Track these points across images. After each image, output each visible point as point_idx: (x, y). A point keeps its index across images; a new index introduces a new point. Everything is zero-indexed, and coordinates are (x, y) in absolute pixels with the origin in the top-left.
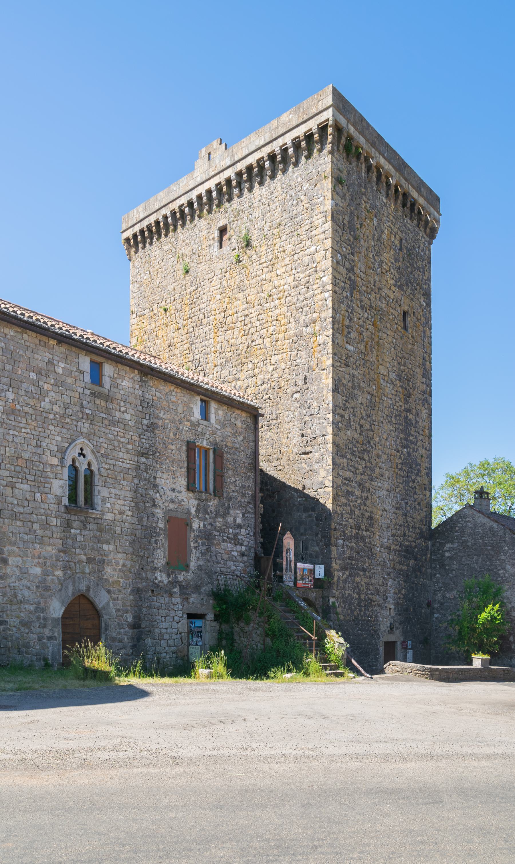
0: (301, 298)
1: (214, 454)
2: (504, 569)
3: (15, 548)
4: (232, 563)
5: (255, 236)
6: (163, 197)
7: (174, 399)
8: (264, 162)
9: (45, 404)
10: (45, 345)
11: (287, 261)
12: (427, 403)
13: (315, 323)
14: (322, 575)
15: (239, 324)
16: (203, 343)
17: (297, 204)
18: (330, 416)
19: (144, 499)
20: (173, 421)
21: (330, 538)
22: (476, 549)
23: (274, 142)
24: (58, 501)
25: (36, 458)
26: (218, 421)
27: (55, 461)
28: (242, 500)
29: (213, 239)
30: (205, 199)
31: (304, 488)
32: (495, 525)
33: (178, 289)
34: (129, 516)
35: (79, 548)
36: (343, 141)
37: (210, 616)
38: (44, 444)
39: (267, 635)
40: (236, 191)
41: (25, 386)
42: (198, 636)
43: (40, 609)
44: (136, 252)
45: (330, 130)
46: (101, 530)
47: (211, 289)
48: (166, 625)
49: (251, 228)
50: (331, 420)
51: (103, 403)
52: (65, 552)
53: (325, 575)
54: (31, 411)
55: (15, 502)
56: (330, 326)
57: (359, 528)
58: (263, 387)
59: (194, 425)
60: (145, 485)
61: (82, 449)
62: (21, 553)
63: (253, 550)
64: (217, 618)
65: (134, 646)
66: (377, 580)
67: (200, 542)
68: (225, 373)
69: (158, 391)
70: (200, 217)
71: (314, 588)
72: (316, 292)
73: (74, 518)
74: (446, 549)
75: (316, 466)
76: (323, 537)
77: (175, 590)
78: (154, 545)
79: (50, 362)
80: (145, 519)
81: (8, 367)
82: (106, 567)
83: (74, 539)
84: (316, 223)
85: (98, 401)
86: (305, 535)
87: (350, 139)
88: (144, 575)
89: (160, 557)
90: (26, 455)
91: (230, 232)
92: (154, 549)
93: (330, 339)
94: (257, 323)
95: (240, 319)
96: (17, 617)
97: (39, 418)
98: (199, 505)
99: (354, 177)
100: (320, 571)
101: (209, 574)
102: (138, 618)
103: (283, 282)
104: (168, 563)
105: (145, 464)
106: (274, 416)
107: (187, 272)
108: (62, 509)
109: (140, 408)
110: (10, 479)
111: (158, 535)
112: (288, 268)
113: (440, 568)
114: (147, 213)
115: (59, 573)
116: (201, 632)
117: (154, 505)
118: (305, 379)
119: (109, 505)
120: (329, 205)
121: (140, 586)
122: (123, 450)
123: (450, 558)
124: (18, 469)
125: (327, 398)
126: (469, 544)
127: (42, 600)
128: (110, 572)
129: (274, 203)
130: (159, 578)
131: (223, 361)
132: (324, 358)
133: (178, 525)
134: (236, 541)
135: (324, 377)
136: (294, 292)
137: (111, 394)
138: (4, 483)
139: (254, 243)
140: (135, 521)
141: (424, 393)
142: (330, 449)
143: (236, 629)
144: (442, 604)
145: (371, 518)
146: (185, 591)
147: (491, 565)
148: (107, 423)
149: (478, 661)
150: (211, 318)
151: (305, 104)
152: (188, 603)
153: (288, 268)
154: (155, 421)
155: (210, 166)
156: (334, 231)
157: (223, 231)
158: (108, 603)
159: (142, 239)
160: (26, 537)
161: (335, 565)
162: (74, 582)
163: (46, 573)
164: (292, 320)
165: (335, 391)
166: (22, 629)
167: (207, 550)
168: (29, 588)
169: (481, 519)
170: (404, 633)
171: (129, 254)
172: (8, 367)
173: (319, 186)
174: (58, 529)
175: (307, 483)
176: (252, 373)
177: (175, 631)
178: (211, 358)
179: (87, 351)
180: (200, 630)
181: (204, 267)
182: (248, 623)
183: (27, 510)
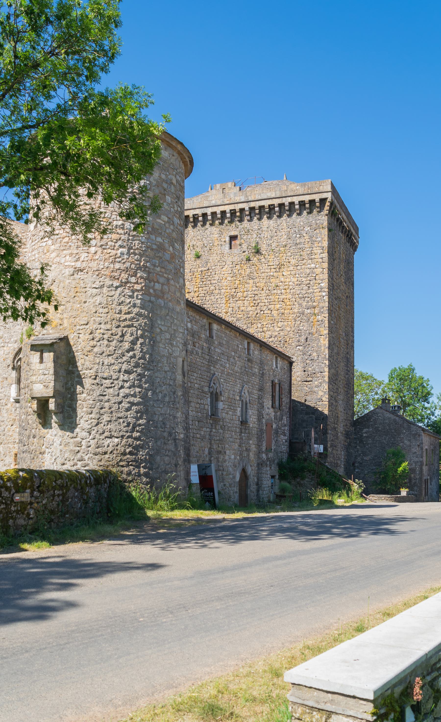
0: (304, 292)
2: (403, 442)
5: (263, 248)
11: (292, 268)
13: (315, 308)
18: (327, 362)
22: (384, 432)
31: (306, 401)
37: (277, 477)
45: (328, 204)
49: (260, 242)
50: (327, 364)
66: (339, 452)
72: (315, 291)
74: (363, 431)
75: (316, 389)
103: (288, 280)
112: (292, 273)
113: (360, 443)
118: (307, 338)
120: (325, 244)
123: (366, 437)
125: (324, 352)
126: (380, 429)
132: (321, 329)
135: (321, 339)
136: (297, 288)
144: (361, 464)
147: (394, 441)
149: (404, 492)
151: (310, 184)
157: (233, 238)
161: (329, 445)
175: (308, 398)
182: (303, 479)
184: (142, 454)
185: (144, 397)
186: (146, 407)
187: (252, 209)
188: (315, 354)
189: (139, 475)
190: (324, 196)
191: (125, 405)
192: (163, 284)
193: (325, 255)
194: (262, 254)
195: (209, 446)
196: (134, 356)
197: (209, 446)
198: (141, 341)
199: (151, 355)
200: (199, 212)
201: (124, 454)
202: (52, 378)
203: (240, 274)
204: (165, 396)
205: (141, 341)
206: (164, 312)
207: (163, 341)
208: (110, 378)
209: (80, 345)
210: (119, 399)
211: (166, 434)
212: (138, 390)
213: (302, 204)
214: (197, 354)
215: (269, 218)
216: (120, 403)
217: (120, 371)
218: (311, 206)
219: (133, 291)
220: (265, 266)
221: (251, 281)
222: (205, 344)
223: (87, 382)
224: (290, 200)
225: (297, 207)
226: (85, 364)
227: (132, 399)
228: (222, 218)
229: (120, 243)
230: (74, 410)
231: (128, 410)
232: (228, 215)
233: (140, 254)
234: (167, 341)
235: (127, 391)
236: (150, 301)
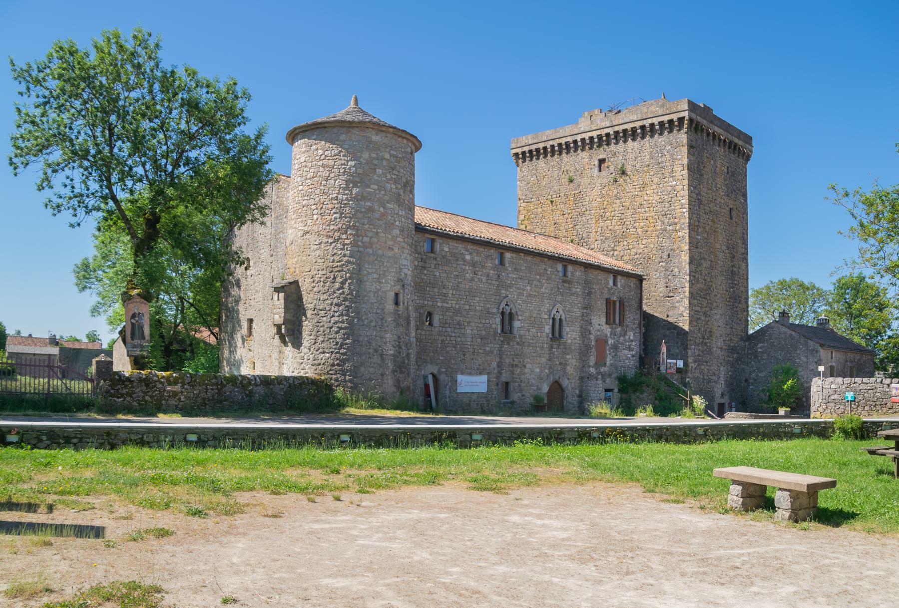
0: (666, 209)
5: (629, 169)
12: (745, 259)
14: (682, 366)
18: (687, 278)
20: (599, 289)
24: (548, 336)
26: (621, 286)
27: (546, 317)
32: (793, 333)
34: (578, 340)
36: (694, 125)
37: (616, 390)
45: (686, 122)
57: (704, 338)
59: (609, 289)
64: (620, 391)
66: (714, 367)
68: (605, 245)
69: (593, 275)
75: (677, 304)
76: (682, 344)
79: (545, 269)
83: (554, 354)
87: (698, 124)
89: (592, 360)
90: (535, 315)
99: (699, 141)
100: (680, 364)
101: (616, 368)
102: (581, 392)
120: (685, 161)
123: (762, 353)
128: (570, 369)
133: (601, 342)
134: (630, 349)
141: (743, 254)
145: (711, 332)
156: (689, 175)
157: (602, 161)
161: (690, 360)
163: (541, 371)
165: (690, 263)
169: (784, 329)
170: (730, 398)
171: (517, 162)
182: (642, 393)
184: (347, 366)
185: (351, 323)
186: (351, 331)
187: (617, 133)
188: (676, 270)
189: (345, 381)
190: (681, 115)
191: (335, 329)
192: (371, 238)
193: (686, 172)
194: (627, 175)
195: (498, 360)
196: (343, 293)
197: (498, 360)
198: (349, 281)
199: (358, 291)
200: (570, 139)
201: (333, 365)
202: (282, 310)
203: (608, 195)
204: (371, 321)
205: (349, 281)
206: (371, 258)
208: (324, 309)
209: (305, 286)
210: (330, 325)
212: (345, 318)
213: (661, 124)
215: (634, 140)
216: (331, 328)
217: (331, 304)
218: (671, 126)
219: (344, 245)
220: (630, 186)
221: (618, 201)
222: (492, 272)
223: (309, 313)
224: (650, 121)
225: (657, 127)
226: (309, 300)
227: (340, 325)
228: (590, 144)
229: (334, 210)
230: (301, 333)
231: (337, 333)
232: (596, 140)
233: (350, 217)
235: (337, 319)
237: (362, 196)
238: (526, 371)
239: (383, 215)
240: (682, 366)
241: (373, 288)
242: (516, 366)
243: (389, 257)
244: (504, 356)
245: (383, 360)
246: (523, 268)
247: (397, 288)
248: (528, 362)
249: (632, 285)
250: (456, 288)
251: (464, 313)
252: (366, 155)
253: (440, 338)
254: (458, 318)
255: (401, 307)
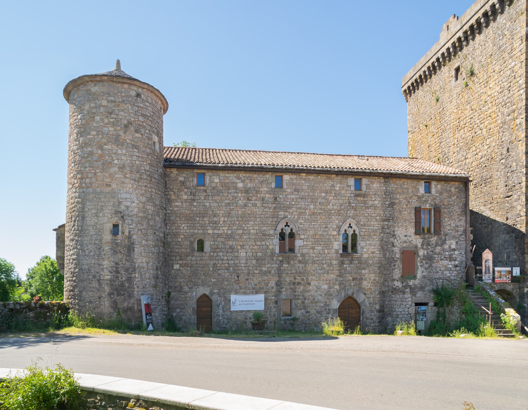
0: (505, 98)
1: (434, 211)
3: (314, 277)
4: (448, 272)
6: (423, 60)
7: (406, 186)
8: (480, 19)
9: (330, 207)
10: (330, 178)
13: (514, 112)
14: (519, 274)
15: (467, 124)
16: (447, 141)
17: (503, 38)
18: (524, 170)
19: (387, 244)
20: (406, 198)
21: (524, 249)
23: (487, 5)
25: (325, 233)
26: (437, 192)
27: (335, 233)
28: (456, 234)
29: (452, 76)
30: (446, 54)
33: (433, 112)
34: (378, 254)
35: (348, 273)
37: (431, 304)
38: (329, 226)
39: (463, 313)
40: (464, 43)
41: (319, 200)
42: (423, 315)
43: (326, 305)
44: (410, 97)
46: (361, 263)
47: (451, 107)
48: (400, 310)
50: (525, 172)
51: (362, 199)
52: (340, 276)
53: (521, 273)
54: (323, 211)
55: (315, 256)
56: (524, 111)
58: (482, 160)
59: (419, 198)
60: (387, 236)
61: (350, 224)
62: (317, 279)
63: (464, 263)
64: (436, 305)
65: (379, 322)
67: (424, 262)
68: (460, 155)
69: (394, 185)
70: (444, 65)
71: (512, 282)
72: (515, 92)
73: (345, 259)
75: (515, 204)
76: (520, 249)
77: (407, 290)
78: (393, 267)
80: (388, 254)
81: (311, 194)
82: (363, 281)
83: (345, 269)
84: (515, 46)
85: (359, 198)
86: (508, 249)
88: (387, 284)
89: (397, 273)
90: (320, 233)
91: (462, 69)
92: (393, 269)
93: (524, 120)
94: (478, 121)
95: (468, 121)
96: (315, 309)
97: (326, 214)
98: (423, 241)
103: (493, 91)
104: (402, 276)
105: (387, 225)
106: (488, 177)
107: (438, 100)
108: (339, 256)
109: (384, 196)
110: (312, 245)
111: (396, 261)
114: (415, 73)
115: (337, 287)
116: (425, 313)
117: (393, 246)
118: (508, 149)
119: (365, 250)
121: (384, 290)
122: (374, 220)
124: (316, 240)
125: (522, 159)
127: (328, 301)
129: (488, 42)
130: (396, 285)
131: (458, 149)
132: (519, 134)
134: (451, 258)
135: (520, 145)
136: (501, 96)
137: (367, 193)
138: (309, 248)
139: (476, 72)
140: (381, 256)
142: (524, 191)
143: (447, 310)
146: (413, 290)
148: (364, 208)
150: (451, 125)
152: (416, 297)
153: (497, 82)
154: (394, 201)
155: (448, 34)
157: (457, 70)
158: (364, 300)
159: (411, 90)
160: (320, 271)
162: (345, 291)
163: (330, 288)
164: (499, 114)
166: (317, 315)
167: (429, 266)
168: (321, 295)
171: (407, 99)
172: (311, 194)
173: (517, 21)
174: (337, 266)
176: (475, 153)
177: (407, 313)
178: (451, 149)
179: (352, 175)
180: (424, 312)
181: (447, 95)
183: (321, 258)
192: (91, 178)
206: (91, 196)
207: (90, 216)
211: (90, 277)
214: (255, 205)
221: (468, 107)
222: (267, 196)
234: (93, 215)
236: (83, 192)
237: (86, 144)
238: (311, 288)
239: (101, 156)
240: (175, 268)
241: (92, 223)
242: (299, 283)
243: (107, 193)
244: (284, 275)
245: (100, 284)
246: (305, 188)
247: (115, 220)
248: (312, 280)
249: (453, 189)
250: (229, 215)
251: (237, 237)
252: (87, 107)
253: (212, 262)
254: (230, 243)
255: (120, 236)
